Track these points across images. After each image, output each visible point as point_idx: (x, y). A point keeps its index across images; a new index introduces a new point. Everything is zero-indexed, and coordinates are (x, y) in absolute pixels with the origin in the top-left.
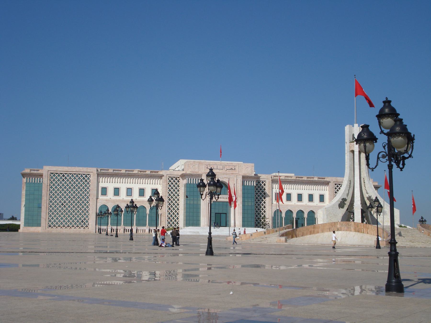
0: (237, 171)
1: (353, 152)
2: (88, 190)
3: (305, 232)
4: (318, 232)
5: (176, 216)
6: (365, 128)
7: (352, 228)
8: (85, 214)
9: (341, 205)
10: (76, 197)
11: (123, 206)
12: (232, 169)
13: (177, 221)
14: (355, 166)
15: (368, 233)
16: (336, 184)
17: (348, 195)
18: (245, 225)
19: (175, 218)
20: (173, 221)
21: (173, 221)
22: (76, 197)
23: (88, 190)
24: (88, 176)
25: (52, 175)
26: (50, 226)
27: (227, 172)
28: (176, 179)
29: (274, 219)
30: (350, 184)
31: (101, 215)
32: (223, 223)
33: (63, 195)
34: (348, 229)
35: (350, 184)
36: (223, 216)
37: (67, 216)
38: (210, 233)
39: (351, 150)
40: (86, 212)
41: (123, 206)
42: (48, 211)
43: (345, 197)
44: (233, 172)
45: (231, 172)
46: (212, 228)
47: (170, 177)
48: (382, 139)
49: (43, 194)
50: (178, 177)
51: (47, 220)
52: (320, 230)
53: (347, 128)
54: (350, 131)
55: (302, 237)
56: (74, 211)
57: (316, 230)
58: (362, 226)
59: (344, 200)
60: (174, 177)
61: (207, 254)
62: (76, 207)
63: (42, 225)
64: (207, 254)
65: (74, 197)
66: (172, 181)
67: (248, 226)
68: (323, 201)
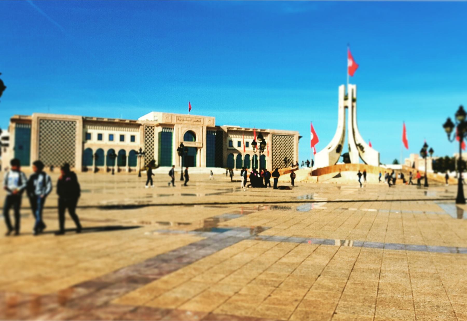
12: (198, 121)
27: (195, 123)
28: (152, 128)
45: (197, 123)
48: (323, 302)
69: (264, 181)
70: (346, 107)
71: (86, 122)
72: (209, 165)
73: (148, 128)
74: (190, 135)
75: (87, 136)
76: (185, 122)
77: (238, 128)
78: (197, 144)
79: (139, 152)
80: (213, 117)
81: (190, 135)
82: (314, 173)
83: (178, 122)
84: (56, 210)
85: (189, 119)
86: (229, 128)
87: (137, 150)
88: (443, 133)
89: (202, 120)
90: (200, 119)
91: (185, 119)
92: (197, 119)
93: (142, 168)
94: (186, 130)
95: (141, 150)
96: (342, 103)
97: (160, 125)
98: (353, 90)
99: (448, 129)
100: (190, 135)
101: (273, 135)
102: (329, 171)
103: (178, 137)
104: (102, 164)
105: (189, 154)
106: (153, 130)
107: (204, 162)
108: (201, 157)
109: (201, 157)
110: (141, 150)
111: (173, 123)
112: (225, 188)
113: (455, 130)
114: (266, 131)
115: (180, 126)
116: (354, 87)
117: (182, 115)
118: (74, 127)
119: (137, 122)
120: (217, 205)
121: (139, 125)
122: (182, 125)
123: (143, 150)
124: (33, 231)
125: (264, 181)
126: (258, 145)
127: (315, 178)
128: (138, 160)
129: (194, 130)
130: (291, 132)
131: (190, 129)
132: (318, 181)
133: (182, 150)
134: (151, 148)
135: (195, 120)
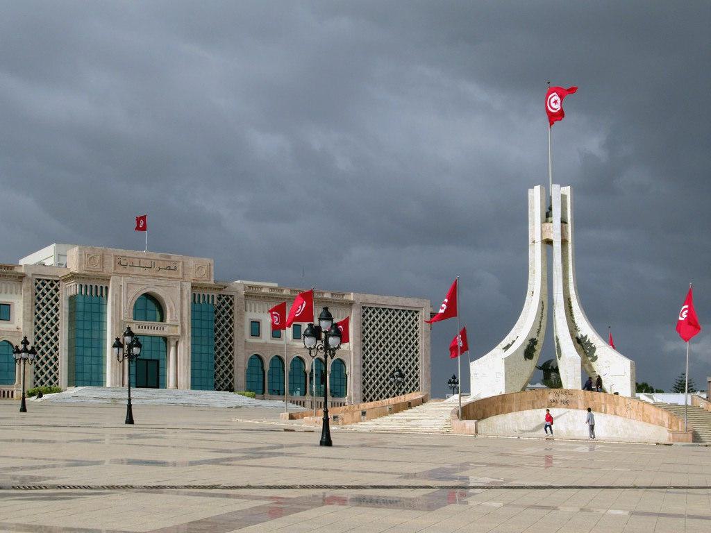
0: (181, 272)
1: (549, 242)
4: (510, 411)
9: (529, 353)
12: (169, 268)
13: (55, 373)
15: (615, 414)
16: (363, 308)
27: (161, 273)
28: (52, 285)
30: (543, 309)
31: (25, 350)
35: (543, 309)
38: (130, 400)
40: (101, 340)
43: (534, 336)
46: (132, 389)
47: (39, 280)
50: (57, 281)
57: (507, 406)
58: (603, 398)
59: (533, 342)
60: (48, 281)
61: (322, 444)
64: (322, 444)
69: (619, 512)
70: (549, 242)
72: (198, 383)
73: (43, 284)
74: (151, 305)
76: (137, 271)
77: (271, 288)
78: (166, 329)
79: (21, 347)
80: (207, 261)
81: (151, 305)
82: (466, 413)
83: (120, 270)
84: (684, 404)
86: (250, 287)
87: (17, 342)
89: (180, 266)
90: (175, 262)
92: (168, 264)
93: (29, 387)
94: (139, 290)
95: (25, 342)
96: (535, 230)
97: (73, 276)
98: (563, 197)
100: (151, 305)
101: (366, 309)
103: (117, 313)
105: (147, 356)
106: (57, 290)
107: (185, 378)
108: (178, 366)
109: (178, 366)
110: (25, 342)
111: (105, 273)
112: (238, 446)
115: (123, 281)
116: (567, 190)
117: (129, 253)
119: (17, 270)
120: (213, 491)
121: (21, 278)
122: (128, 279)
123: (31, 340)
124: (319, 443)
125: (619, 512)
127: (470, 424)
128: (19, 368)
129: (159, 292)
130: (411, 303)
131: (148, 290)
132: (477, 432)
133: (130, 344)
134: (52, 338)
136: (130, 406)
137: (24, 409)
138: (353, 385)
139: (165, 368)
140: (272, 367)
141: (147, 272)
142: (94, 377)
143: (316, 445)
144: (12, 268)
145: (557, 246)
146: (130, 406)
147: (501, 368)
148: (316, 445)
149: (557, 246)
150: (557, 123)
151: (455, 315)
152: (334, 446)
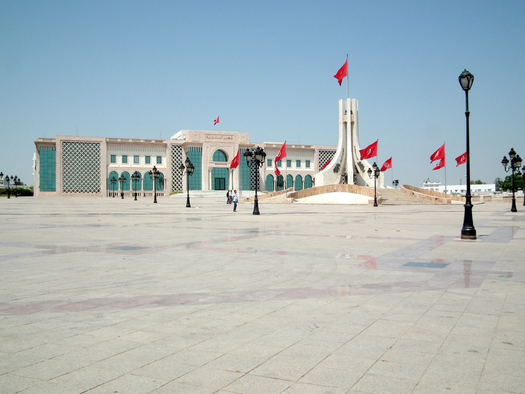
1: (345, 123)
2: (98, 158)
3: (307, 194)
5: (179, 181)
6: (505, 157)
7: (347, 189)
8: (97, 180)
10: (88, 164)
11: (131, 173)
14: (348, 136)
17: (341, 161)
18: (243, 188)
19: (179, 183)
20: (177, 185)
21: (177, 185)
22: (88, 164)
23: (98, 158)
24: (98, 145)
25: (64, 144)
26: (65, 191)
27: (225, 141)
29: (267, 182)
32: (222, 187)
33: (75, 162)
34: (343, 190)
36: (222, 181)
37: (80, 181)
38: (188, 195)
39: (345, 121)
40: (97, 178)
41: (143, 173)
42: (62, 177)
43: (339, 163)
44: (231, 141)
45: (228, 141)
48: (510, 162)
49: (57, 162)
51: (62, 185)
52: (319, 192)
53: (341, 102)
54: (344, 105)
55: (304, 198)
56: (86, 177)
62: (88, 173)
63: (57, 190)
65: (86, 164)
66: (175, 149)
67: (244, 189)
68: (161, 163)
71: (110, 143)
75: (113, 159)
76: (215, 140)
81: (221, 155)
83: (208, 140)
85: (220, 137)
88: (502, 166)
90: (232, 136)
91: (214, 137)
92: (229, 136)
94: (215, 149)
99: (505, 164)
100: (221, 154)
102: (316, 192)
104: (128, 189)
111: (201, 142)
113: (509, 164)
114: (312, 147)
118: (98, 149)
126: (373, 172)
131: (219, 148)
135: (226, 137)
136: (188, 198)
137: (155, 202)
138: (285, 185)
139: (228, 181)
140: (306, 179)
141: (219, 140)
142: (197, 186)
143: (249, 214)
144: (162, 141)
145: (349, 125)
146: (188, 198)
147: (323, 177)
148: (249, 214)
149: (349, 125)
150: (345, 79)
151: (456, 159)
152: (520, 211)
